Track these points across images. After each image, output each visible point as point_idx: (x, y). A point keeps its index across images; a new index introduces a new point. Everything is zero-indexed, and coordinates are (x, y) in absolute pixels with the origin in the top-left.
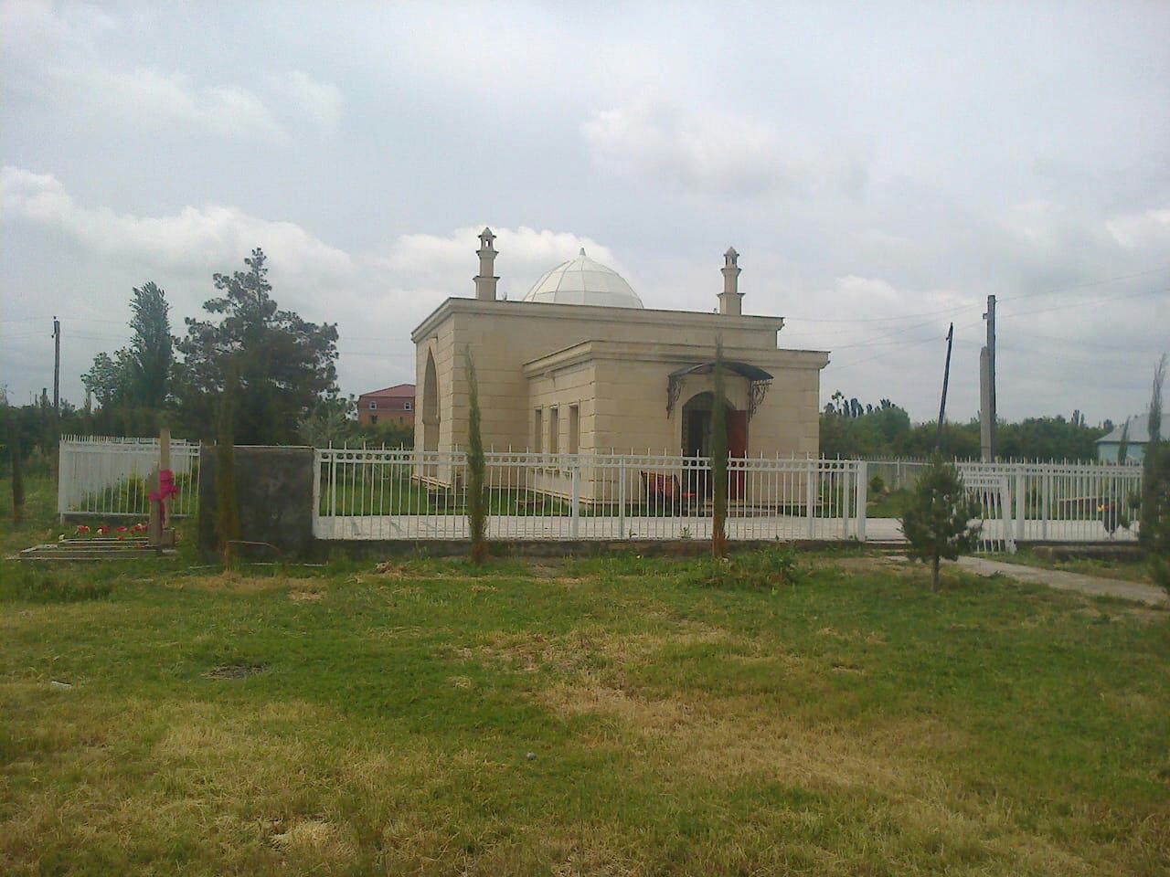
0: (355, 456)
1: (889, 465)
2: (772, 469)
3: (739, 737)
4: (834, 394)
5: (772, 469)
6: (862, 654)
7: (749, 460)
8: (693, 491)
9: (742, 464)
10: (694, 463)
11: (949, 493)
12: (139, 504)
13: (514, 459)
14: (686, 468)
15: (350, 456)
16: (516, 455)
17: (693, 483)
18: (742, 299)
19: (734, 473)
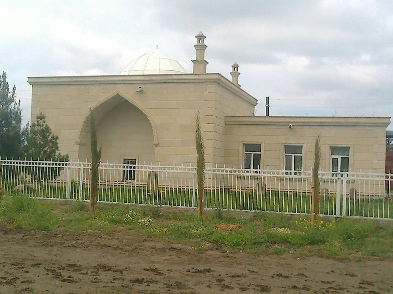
0: (220, 171)
1: (272, 180)
2: (112, 168)
3: (139, 263)
4: (206, 42)
5: (112, 168)
6: (355, 281)
7: (260, 170)
8: (39, 176)
9: (134, 167)
10: (49, 164)
11: (12, 121)
12: (26, 169)
13: (131, 167)
14: (388, 180)
15: (46, 164)
16: (110, 164)
17: (39, 172)
18: (207, 66)
19: (130, 171)
